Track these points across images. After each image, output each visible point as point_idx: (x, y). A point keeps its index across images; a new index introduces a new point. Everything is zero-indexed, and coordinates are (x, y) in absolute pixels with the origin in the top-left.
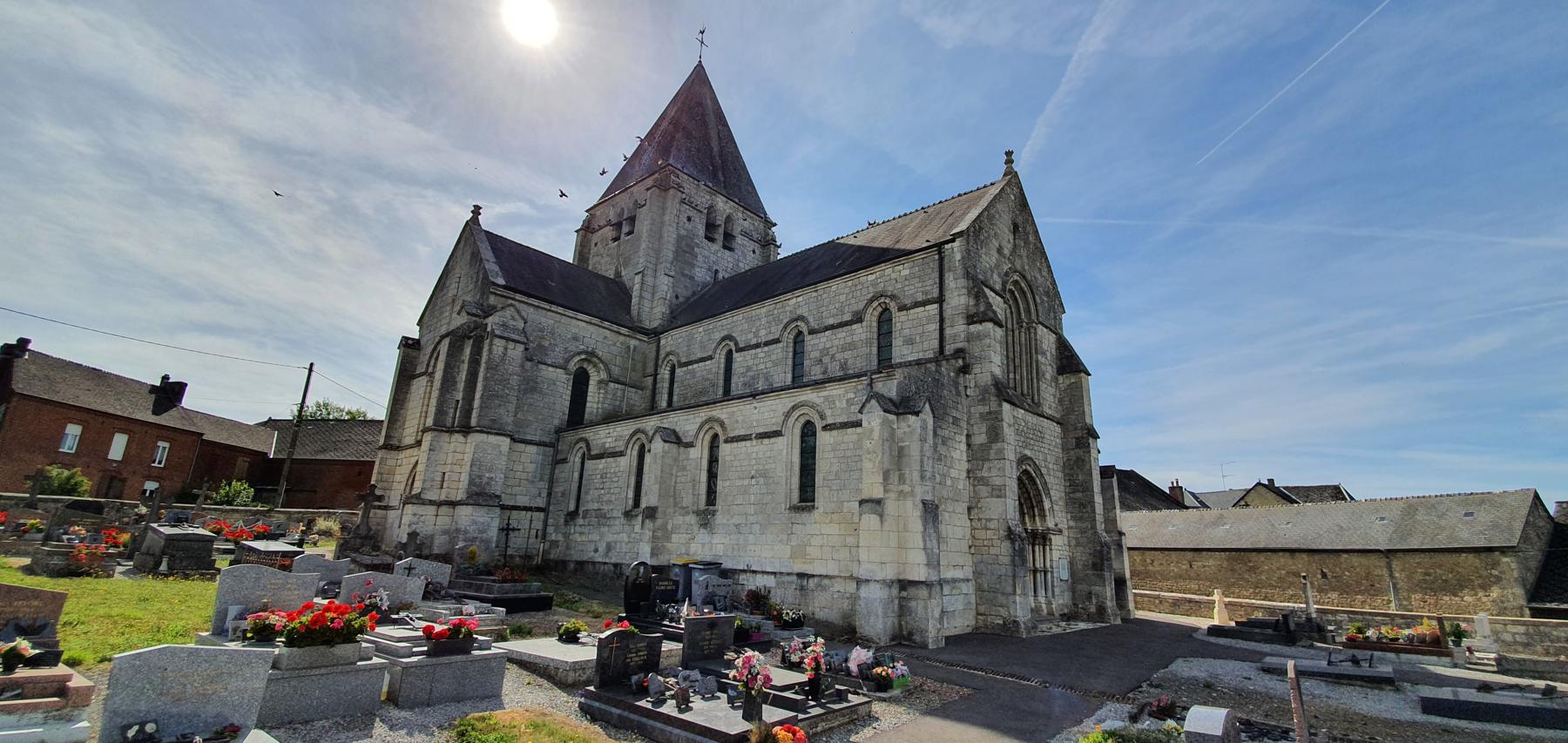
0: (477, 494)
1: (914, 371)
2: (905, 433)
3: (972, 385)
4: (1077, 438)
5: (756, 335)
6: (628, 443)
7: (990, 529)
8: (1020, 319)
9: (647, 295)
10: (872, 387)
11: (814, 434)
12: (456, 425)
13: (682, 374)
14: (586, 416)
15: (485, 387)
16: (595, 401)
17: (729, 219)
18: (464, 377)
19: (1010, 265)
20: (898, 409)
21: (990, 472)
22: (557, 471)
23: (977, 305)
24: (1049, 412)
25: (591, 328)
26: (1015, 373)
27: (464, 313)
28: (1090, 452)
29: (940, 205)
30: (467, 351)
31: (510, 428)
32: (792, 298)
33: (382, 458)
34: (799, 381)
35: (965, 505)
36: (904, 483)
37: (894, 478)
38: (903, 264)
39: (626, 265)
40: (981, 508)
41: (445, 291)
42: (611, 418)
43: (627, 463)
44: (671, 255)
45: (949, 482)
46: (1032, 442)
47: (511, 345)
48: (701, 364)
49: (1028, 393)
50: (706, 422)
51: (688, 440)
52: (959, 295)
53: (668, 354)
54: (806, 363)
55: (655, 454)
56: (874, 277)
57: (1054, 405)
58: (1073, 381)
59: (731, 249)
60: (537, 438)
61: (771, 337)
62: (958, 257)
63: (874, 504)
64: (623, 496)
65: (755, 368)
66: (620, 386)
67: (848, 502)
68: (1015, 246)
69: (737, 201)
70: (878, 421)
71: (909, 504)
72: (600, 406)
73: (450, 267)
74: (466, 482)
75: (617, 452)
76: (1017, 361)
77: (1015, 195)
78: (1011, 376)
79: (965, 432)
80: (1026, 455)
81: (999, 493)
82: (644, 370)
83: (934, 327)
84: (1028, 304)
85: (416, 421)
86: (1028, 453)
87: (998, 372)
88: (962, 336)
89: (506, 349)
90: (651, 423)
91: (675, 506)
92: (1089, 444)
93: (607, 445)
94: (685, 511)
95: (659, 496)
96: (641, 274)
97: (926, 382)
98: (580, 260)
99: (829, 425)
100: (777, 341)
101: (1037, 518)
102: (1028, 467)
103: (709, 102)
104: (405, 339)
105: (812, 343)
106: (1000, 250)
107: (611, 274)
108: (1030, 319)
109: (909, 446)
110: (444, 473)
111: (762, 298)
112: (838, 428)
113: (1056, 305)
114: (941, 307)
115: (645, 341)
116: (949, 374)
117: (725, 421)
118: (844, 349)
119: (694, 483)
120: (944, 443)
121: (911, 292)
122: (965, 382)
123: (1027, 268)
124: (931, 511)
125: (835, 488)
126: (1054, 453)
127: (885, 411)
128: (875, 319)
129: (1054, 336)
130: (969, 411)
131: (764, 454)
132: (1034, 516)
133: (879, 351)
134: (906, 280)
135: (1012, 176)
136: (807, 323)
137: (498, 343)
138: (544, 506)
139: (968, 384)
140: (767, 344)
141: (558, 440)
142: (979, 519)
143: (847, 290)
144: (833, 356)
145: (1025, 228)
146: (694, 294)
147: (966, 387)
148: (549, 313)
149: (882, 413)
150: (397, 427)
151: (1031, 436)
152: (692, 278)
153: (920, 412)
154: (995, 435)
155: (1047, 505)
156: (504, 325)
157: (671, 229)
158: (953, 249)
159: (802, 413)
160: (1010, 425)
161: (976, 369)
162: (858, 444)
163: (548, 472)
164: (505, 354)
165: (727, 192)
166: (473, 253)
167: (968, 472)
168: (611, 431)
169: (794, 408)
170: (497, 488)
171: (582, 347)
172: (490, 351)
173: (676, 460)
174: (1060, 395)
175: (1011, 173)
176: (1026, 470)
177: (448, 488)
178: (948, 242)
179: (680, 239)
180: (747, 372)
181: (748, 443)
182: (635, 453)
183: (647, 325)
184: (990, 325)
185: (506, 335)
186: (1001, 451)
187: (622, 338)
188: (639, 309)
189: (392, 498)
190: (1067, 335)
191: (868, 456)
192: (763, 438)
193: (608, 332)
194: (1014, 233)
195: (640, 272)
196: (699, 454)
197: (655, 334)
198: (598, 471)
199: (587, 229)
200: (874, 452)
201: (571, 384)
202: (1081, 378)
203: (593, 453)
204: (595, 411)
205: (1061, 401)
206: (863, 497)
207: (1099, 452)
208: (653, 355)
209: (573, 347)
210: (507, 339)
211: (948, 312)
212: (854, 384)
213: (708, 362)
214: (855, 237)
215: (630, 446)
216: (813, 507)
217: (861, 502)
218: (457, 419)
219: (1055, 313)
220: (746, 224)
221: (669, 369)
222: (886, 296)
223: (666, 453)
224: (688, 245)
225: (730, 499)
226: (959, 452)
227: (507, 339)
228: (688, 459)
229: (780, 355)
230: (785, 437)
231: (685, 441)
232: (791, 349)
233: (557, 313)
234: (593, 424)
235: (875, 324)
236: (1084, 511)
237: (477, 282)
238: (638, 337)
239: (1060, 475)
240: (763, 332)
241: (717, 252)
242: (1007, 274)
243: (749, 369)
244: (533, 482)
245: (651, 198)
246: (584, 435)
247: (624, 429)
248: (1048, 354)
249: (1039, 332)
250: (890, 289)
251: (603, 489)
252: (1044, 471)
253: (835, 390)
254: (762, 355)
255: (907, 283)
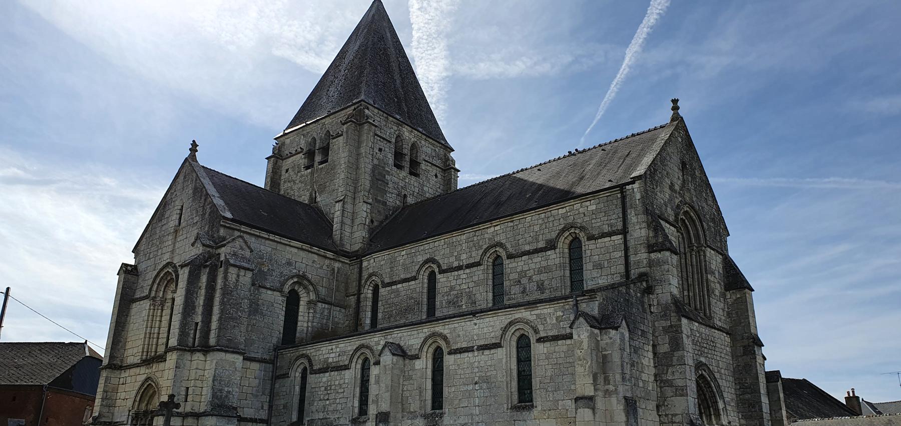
0: (219, 406)
1: (610, 294)
2: (607, 344)
3: (655, 303)
4: (745, 346)
5: (458, 258)
6: (352, 356)
7: (675, 423)
8: (691, 243)
9: (348, 221)
10: (577, 308)
11: (529, 346)
12: (196, 345)
13: (386, 293)
14: (298, 335)
15: (222, 312)
16: (305, 321)
17: (414, 147)
18: (201, 303)
19: (680, 199)
20: (601, 325)
21: (673, 375)
22: (277, 386)
23: (656, 236)
24: (719, 324)
25: (302, 253)
26: (688, 290)
27: (199, 245)
28: (755, 358)
29: (616, 144)
30: (204, 279)
31: (242, 347)
32: (490, 227)
33: (107, 378)
34: (499, 303)
35: (654, 403)
36: (609, 384)
37: (601, 380)
38: (590, 200)
39: (322, 189)
40: (667, 406)
41: (164, 221)
42: (322, 335)
43: (351, 376)
44: (368, 184)
45: (641, 384)
46: (706, 351)
47: (242, 273)
48: (404, 284)
49: (701, 307)
50: (430, 336)
51: (413, 353)
52: (640, 229)
53: (370, 276)
54: (506, 283)
55: (385, 366)
56: (564, 210)
57: (723, 318)
58: (738, 296)
59: (416, 175)
60: (258, 356)
61: (472, 261)
62: (638, 196)
63: (587, 401)
64: (349, 405)
65: (458, 288)
66: (327, 306)
67: (562, 400)
68: (684, 181)
69: (421, 130)
70: (586, 334)
71: (614, 400)
72: (310, 324)
73: (167, 199)
74: (210, 395)
75: (342, 366)
76: (690, 280)
77: (681, 138)
78: (686, 293)
79: (651, 342)
80: (701, 362)
81: (681, 392)
82: (346, 290)
83: (620, 255)
84: (697, 230)
85: (140, 342)
86: (703, 359)
87: (675, 291)
88: (645, 262)
89: (238, 276)
90: (377, 340)
91: (402, 411)
92: (755, 351)
93: (330, 360)
94: (413, 415)
95: (391, 402)
96: (342, 202)
97: (619, 302)
98: (271, 186)
99: (541, 338)
100: (478, 264)
101: (713, 417)
102: (704, 373)
103: (388, 35)
104: (124, 265)
105: (510, 266)
106: (671, 187)
107: (305, 199)
108: (700, 243)
109: (611, 354)
110: (188, 388)
111: (460, 226)
112: (550, 341)
113: (722, 232)
114: (625, 238)
115: (347, 263)
116: (636, 295)
117: (448, 335)
118: (540, 272)
119: (421, 391)
120: (636, 352)
121: (598, 224)
122: (649, 301)
123: (694, 199)
124: (631, 405)
125: (550, 390)
126: (724, 360)
127: (591, 327)
128: (566, 246)
129: (721, 256)
130: (654, 325)
131: (485, 363)
132: (710, 415)
133: (571, 274)
134: (593, 214)
135: (677, 118)
136: (505, 249)
137: (233, 271)
138: (266, 418)
139: (652, 303)
140: (469, 266)
141: (276, 357)
142: (666, 415)
143: (540, 222)
144: (530, 278)
145: (691, 165)
146: (387, 217)
147: (650, 305)
148: (267, 242)
149: (589, 328)
150: (119, 347)
151: (705, 345)
152: (384, 204)
153: (619, 327)
154: (676, 344)
155: (721, 405)
156: (235, 254)
157: (367, 161)
158: (633, 189)
159: (517, 327)
160: (688, 337)
161: (658, 290)
162: (570, 352)
163: (268, 387)
164: (237, 281)
165: (411, 122)
166: (195, 190)
167: (656, 375)
168: (334, 347)
169: (511, 324)
170: (234, 402)
171: (294, 271)
172: (225, 278)
173: (403, 371)
174: (728, 308)
175: (677, 119)
176: (702, 374)
177: (193, 401)
178: (628, 184)
179: (375, 168)
180: (450, 291)
181: (470, 354)
182: (359, 366)
183: (348, 248)
184: (668, 253)
185: (238, 263)
186: (683, 357)
187: (327, 262)
188: (342, 234)
189: (116, 414)
190: (731, 254)
191: (579, 362)
192: (484, 349)
193: (316, 256)
194: (683, 171)
195: (341, 200)
196: (424, 364)
197: (357, 257)
198: (321, 384)
199: (278, 156)
200: (585, 359)
201: (285, 305)
202: (745, 293)
203: (315, 368)
204: (305, 329)
205: (729, 314)
206: (577, 395)
207: (765, 359)
208: (355, 276)
209: (286, 271)
210: (240, 267)
211: (631, 243)
212: (562, 304)
213: (413, 282)
214: (539, 170)
215: (355, 360)
216: (532, 406)
217: (577, 399)
218: (197, 340)
219: (721, 236)
220: (429, 151)
221: (371, 288)
222: (575, 228)
223: (394, 365)
224: (380, 174)
225: (456, 402)
226: (647, 359)
227: (240, 267)
228: (413, 369)
229: (482, 277)
230: (504, 348)
231: (409, 354)
232: (491, 271)
233: (274, 241)
234: (305, 343)
235: (567, 251)
236: (753, 410)
237: (204, 214)
238: (341, 259)
239: (731, 379)
240: (464, 257)
241: (404, 179)
242: (678, 207)
243: (452, 288)
244: (257, 396)
245: (347, 132)
246: (304, 352)
247: (348, 346)
248: (717, 273)
249: (708, 255)
250: (579, 221)
251: (328, 399)
252: (717, 375)
253: (546, 310)
254: (465, 276)
255: (594, 216)
